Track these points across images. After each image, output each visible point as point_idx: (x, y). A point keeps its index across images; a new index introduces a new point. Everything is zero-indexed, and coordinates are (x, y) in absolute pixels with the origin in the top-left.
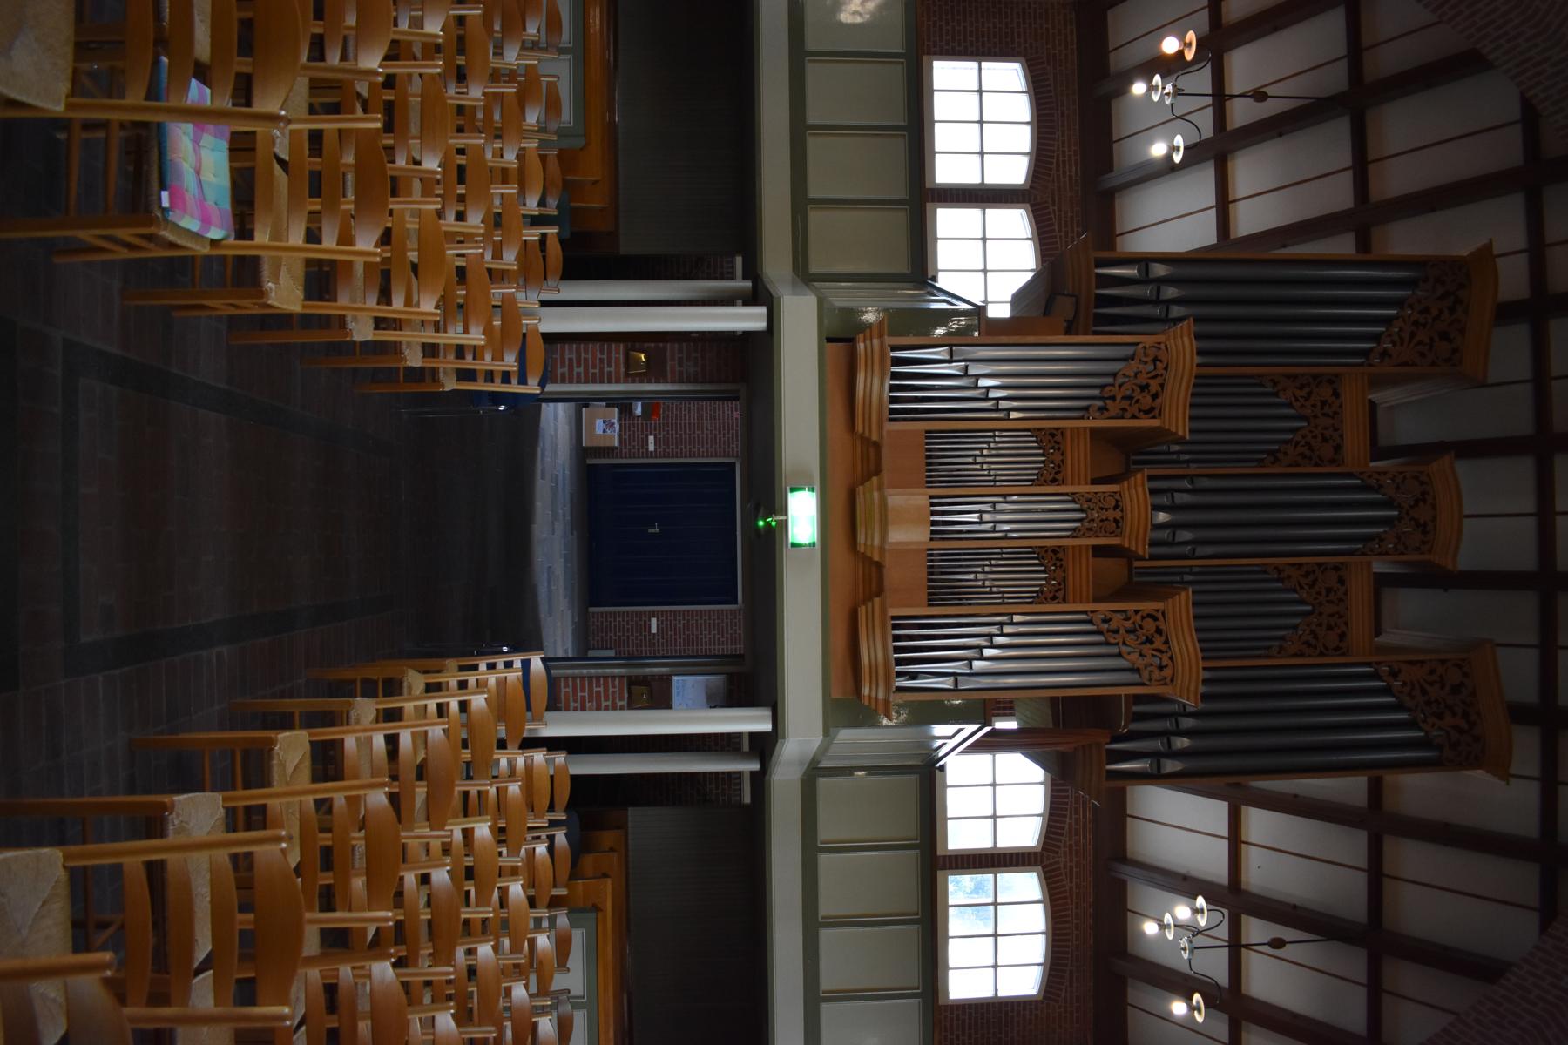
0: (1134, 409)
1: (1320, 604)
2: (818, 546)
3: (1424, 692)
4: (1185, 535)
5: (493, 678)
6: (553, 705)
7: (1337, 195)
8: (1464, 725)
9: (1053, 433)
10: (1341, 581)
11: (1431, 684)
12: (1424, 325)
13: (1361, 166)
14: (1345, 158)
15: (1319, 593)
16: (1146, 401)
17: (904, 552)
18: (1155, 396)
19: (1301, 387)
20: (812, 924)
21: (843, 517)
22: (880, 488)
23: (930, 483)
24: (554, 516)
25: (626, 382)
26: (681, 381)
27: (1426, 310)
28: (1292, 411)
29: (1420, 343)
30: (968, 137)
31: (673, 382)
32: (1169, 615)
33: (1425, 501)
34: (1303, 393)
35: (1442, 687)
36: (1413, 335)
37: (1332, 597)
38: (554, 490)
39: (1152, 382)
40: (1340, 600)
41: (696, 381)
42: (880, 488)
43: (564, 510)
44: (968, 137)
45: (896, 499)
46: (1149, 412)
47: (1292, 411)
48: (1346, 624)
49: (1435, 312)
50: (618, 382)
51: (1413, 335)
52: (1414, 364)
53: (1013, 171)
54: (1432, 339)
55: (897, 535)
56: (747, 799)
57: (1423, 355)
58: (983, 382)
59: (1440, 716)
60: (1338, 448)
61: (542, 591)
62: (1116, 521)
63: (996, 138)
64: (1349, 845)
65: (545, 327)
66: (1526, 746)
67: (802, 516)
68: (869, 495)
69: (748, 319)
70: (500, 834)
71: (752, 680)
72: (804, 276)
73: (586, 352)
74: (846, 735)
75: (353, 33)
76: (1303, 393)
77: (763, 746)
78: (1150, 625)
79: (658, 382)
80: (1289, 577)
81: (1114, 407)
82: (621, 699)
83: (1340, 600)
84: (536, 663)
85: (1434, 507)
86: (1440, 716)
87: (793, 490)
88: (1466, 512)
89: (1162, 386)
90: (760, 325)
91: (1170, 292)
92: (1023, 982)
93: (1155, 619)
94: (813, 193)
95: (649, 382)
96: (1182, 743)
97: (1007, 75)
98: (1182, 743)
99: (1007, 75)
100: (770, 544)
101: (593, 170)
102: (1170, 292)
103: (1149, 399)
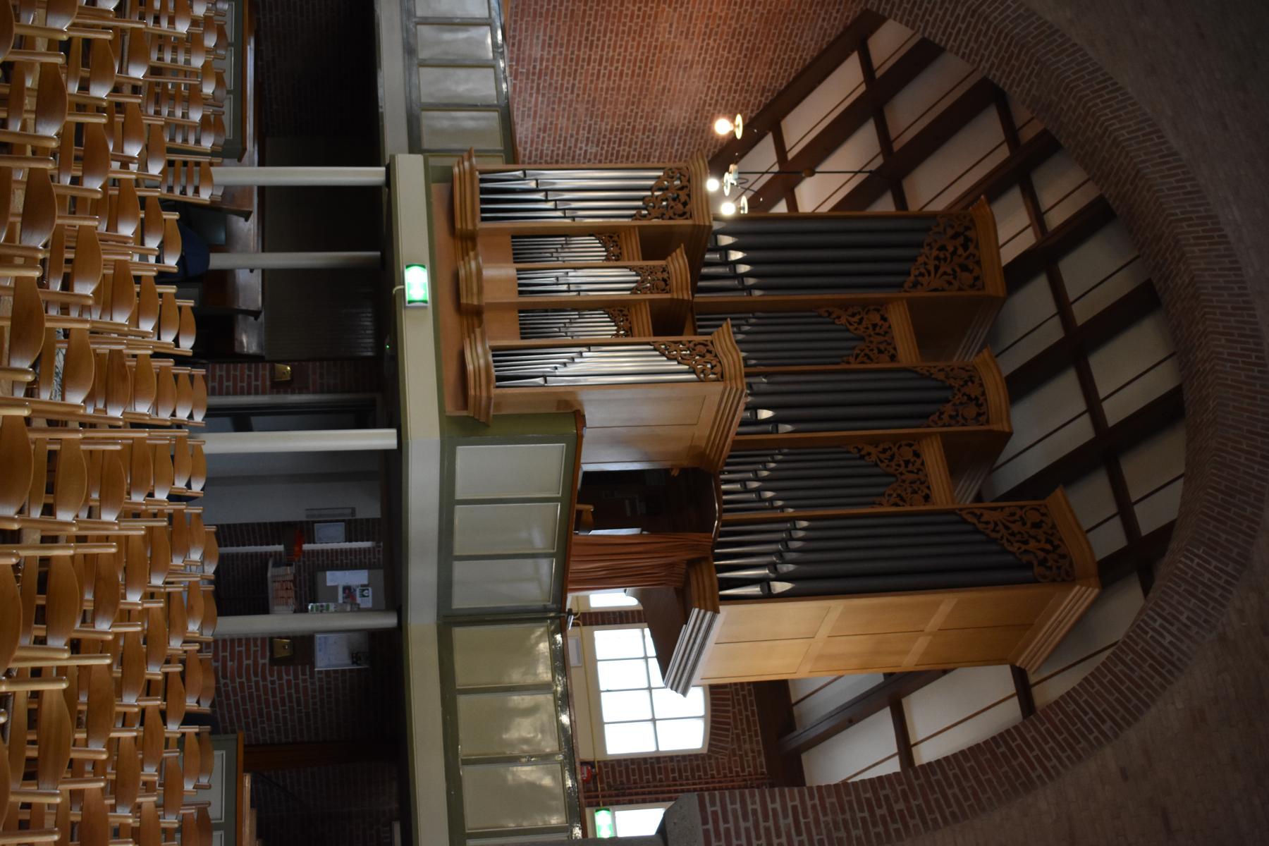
0: (671, 213)
1: (901, 474)
2: (429, 305)
3: (1007, 528)
8: (1048, 547)
11: (1014, 522)
12: (945, 259)
15: (899, 465)
18: (685, 204)
19: (853, 315)
22: (476, 258)
25: (271, 393)
26: (322, 392)
28: (847, 335)
29: (945, 273)
31: (315, 392)
32: (717, 343)
33: (973, 382)
34: (856, 319)
35: (1024, 524)
36: (937, 268)
37: (910, 467)
39: (680, 193)
40: (919, 470)
41: (335, 392)
42: (476, 258)
46: (682, 215)
47: (847, 335)
48: (928, 488)
49: (951, 249)
50: (264, 393)
51: (937, 268)
52: (943, 290)
54: (954, 271)
57: (950, 283)
58: (550, 205)
62: (664, 280)
67: (416, 283)
69: (382, 439)
72: (414, 146)
73: (235, 370)
75: (19, 219)
76: (856, 319)
79: (300, 392)
80: (869, 454)
81: (656, 212)
82: (263, 657)
83: (919, 470)
85: (981, 385)
87: (408, 266)
88: (1085, 528)
89: (689, 195)
93: (706, 345)
95: (293, 392)
103: (680, 206)
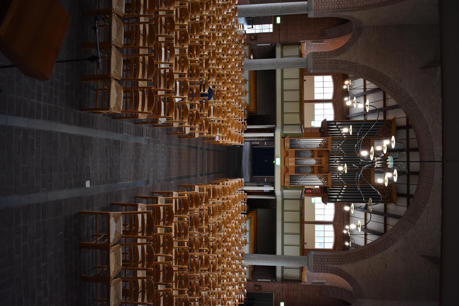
5: (237, 181)
6: (245, 186)
7: (380, 105)
9: (313, 150)
10: (370, 172)
13: (385, 100)
14: (382, 98)
16: (325, 146)
17: (291, 166)
21: (284, 162)
24: (246, 158)
27: (384, 128)
38: (246, 154)
43: (248, 157)
44: (321, 90)
45: (290, 159)
46: (326, 148)
53: (330, 96)
55: (290, 164)
59: (385, 194)
61: (244, 172)
64: (381, 219)
65: (245, 136)
66: (404, 201)
67: (278, 161)
68: (287, 159)
70: (227, 250)
71: (272, 184)
74: (285, 191)
77: (272, 193)
78: (325, 177)
84: (243, 180)
86: (385, 194)
90: (273, 136)
92: (330, 246)
99: (329, 79)
100: (273, 166)
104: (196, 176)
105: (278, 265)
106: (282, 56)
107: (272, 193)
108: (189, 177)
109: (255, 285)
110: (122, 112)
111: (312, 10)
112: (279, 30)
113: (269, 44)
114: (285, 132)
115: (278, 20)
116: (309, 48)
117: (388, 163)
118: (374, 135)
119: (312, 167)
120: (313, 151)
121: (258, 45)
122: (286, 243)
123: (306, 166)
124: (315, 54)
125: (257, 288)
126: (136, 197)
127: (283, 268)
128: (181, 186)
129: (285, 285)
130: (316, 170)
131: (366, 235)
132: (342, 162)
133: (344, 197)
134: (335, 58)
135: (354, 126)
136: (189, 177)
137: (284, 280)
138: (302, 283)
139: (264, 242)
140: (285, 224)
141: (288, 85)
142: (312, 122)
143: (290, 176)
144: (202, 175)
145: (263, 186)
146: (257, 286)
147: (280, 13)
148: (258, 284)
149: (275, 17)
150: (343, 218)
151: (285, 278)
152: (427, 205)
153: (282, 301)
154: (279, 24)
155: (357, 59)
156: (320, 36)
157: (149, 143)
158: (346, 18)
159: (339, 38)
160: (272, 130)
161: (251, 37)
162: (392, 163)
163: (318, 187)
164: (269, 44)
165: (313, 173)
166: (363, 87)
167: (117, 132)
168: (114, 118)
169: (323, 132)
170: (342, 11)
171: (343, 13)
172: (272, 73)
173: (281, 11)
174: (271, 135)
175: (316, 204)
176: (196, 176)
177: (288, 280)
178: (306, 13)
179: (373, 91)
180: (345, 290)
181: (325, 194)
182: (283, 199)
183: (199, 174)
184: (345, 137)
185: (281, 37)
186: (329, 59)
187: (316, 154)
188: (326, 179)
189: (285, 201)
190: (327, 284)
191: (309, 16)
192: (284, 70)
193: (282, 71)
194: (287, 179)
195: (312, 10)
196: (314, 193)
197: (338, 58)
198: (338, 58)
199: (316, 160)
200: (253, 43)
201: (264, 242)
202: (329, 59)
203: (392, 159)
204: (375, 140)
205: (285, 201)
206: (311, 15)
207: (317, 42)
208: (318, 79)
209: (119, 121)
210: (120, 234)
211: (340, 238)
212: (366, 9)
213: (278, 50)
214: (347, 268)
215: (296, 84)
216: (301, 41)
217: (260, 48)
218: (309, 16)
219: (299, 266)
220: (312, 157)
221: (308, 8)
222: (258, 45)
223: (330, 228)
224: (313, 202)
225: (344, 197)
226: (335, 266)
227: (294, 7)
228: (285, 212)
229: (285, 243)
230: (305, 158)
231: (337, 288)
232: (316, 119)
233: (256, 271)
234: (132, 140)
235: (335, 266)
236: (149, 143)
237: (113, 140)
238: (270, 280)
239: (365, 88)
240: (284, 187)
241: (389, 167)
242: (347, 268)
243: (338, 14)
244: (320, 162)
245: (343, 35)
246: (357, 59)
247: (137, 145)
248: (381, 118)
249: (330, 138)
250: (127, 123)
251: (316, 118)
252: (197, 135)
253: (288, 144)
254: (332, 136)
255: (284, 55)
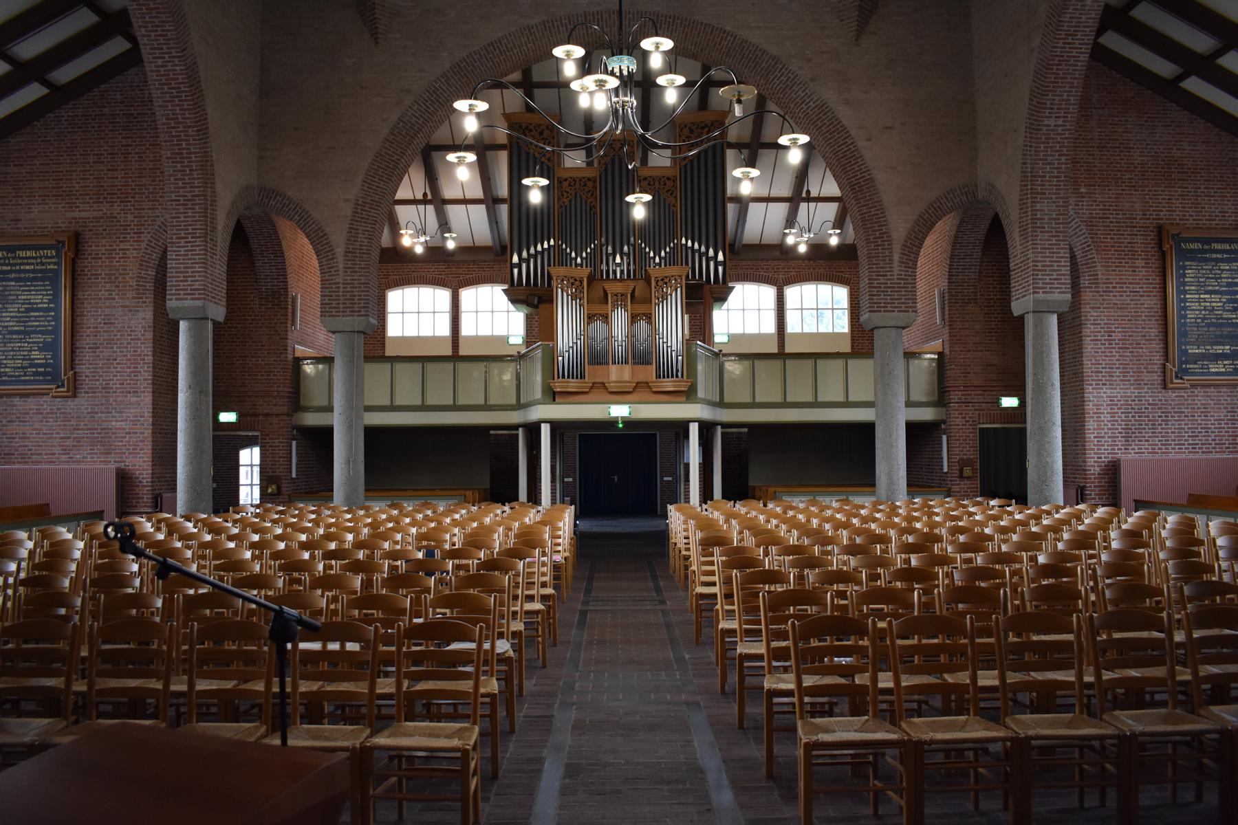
4: (626, 248)
9: (589, 318)
20: (785, 405)
21: (620, 394)
23: (607, 364)
30: (426, 319)
44: (426, 319)
45: (613, 377)
46: (581, 282)
53: (442, 296)
55: (627, 377)
56: (746, 430)
60: (589, 179)
63: (426, 306)
67: (620, 411)
71: (679, 429)
74: (701, 393)
77: (707, 429)
78: (660, 283)
91: (525, 254)
92: (841, 294)
94: (482, 402)
96: (711, 253)
97: (395, 298)
98: (711, 253)
99: (395, 298)
100: (628, 423)
101: (469, 493)
102: (525, 254)
104: (664, 613)
105: (903, 416)
106: (330, 409)
107: (707, 429)
108: (668, 626)
109: (961, 477)
110: (475, 723)
111: (203, 308)
112: (256, 415)
113: (294, 443)
114: (538, 394)
115: (228, 417)
116: (313, 337)
117: (625, 73)
118: (549, 168)
119: (634, 319)
120: (591, 318)
121: (294, 475)
122: (839, 399)
123: (631, 336)
124: (328, 310)
125: (967, 471)
126: (741, 727)
127: (909, 404)
128: (697, 639)
129: (955, 396)
130: (641, 309)
131: (809, 199)
132: (618, 249)
133: (711, 243)
134: (341, 258)
135: (524, 171)
136: (668, 626)
137: (941, 398)
138: (947, 351)
139: (841, 454)
140: (789, 400)
141: (408, 393)
142: (512, 341)
143: (658, 376)
144: (663, 602)
145: (687, 466)
146: (961, 470)
147: (207, 395)
148: (956, 468)
149: (218, 426)
150: (767, 260)
151: (936, 398)
152: (728, 29)
153: (998, 403)
154: (240, 416)
155: (346, 201)
156: (279, 301)
157: (573, 704)
158: (233, 224)
159: (286, 254)
160: (533, 430)
161: (271, 494)
162: (625, 57)
163: (686, 317)
164: (294, 443)
165: (649, 318)
166: (421, 207)
167: (540, 771)
168: (495, 777)
169: (540, 298)
170: (214, 229)
171: (220, 228)
172: (372, 433)
173: (201, 392)
174: (545, 430)
175: (732, 332)
176: (664, 613)
177: (939, 388)
178: (210, 325)
179: (432, 178)
180: (956, 237)
181: (703, 297)
182: (721, 404)
183: (659, 607)
184: (552, 243)
185: (275, 410)
186: (341, 272)
187: (598, 309)
188: (665, 281)
189: (727, 399)
190: (944, 284)
191: (221, 318)
192: (367, 403)
193: (369, 409)
194: (668, 384)
195: (203, 308)
196: (701, 328)
197: (340, 251)
198: (340, 251)
199: (615, 307)
200: (286, 489)
201: (841, 454)
202: (341, 272)
203: (615, 58)
204: (559, 165)
205: (727, 399)
206: (218, 312)
207: (294, 313)
208: (394, 328)
209: (504, 766)
210: (867, 721)
211: (823, 264)
212: (212, 165)
213: (311, 420)
214: (899, 227)
215: (407, 377)
216: (290, 357)
217: (302, 473)
218: (221, 318)
219: (900, 364)
220: (606, 318)
221: (198, 319)
222: (294, 475)
223: (793, 293)
224: (725, 339)
225: (711, 243)
226: (896, 257)
227: (195, 357)
228: (758, 400)
229: (840, 398)
230: (610, 337)
231: (952, 258)
232: (504, 333)
233: (922, 477)
234: (563, 736)
235: (896, 257)
236: (573, 704)
237: (565, 778)
238: (944, 437)
239: (425, 201)
240: (689, 394)
241: (634, 67)
242: (899, 227)
243: (219, 240)
244: (620, 299)
245: (279, 244)
246: (346, 201)
247: (578, 727)
248: (503, 156)
249: (557, 271)
250: (511, 750)
251: (500, 331)
252: (549, 591)
253: (573, 384)
254: (549, 265)
255: (325, 403)
